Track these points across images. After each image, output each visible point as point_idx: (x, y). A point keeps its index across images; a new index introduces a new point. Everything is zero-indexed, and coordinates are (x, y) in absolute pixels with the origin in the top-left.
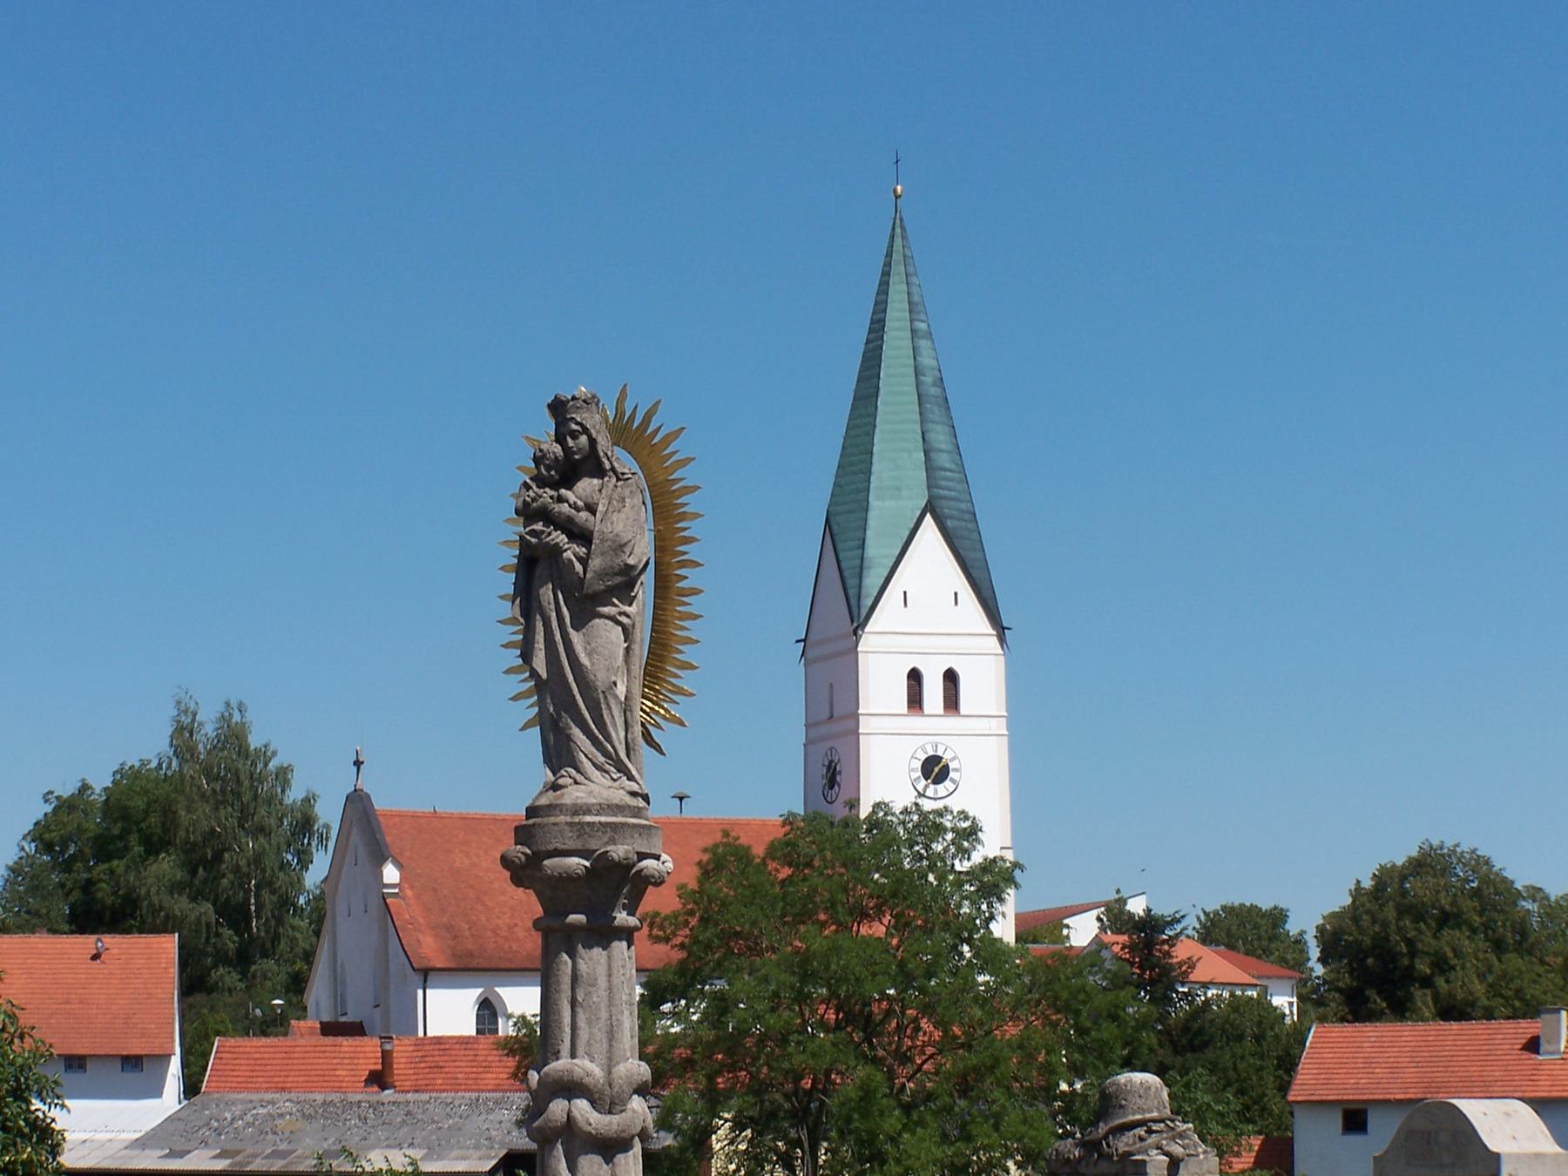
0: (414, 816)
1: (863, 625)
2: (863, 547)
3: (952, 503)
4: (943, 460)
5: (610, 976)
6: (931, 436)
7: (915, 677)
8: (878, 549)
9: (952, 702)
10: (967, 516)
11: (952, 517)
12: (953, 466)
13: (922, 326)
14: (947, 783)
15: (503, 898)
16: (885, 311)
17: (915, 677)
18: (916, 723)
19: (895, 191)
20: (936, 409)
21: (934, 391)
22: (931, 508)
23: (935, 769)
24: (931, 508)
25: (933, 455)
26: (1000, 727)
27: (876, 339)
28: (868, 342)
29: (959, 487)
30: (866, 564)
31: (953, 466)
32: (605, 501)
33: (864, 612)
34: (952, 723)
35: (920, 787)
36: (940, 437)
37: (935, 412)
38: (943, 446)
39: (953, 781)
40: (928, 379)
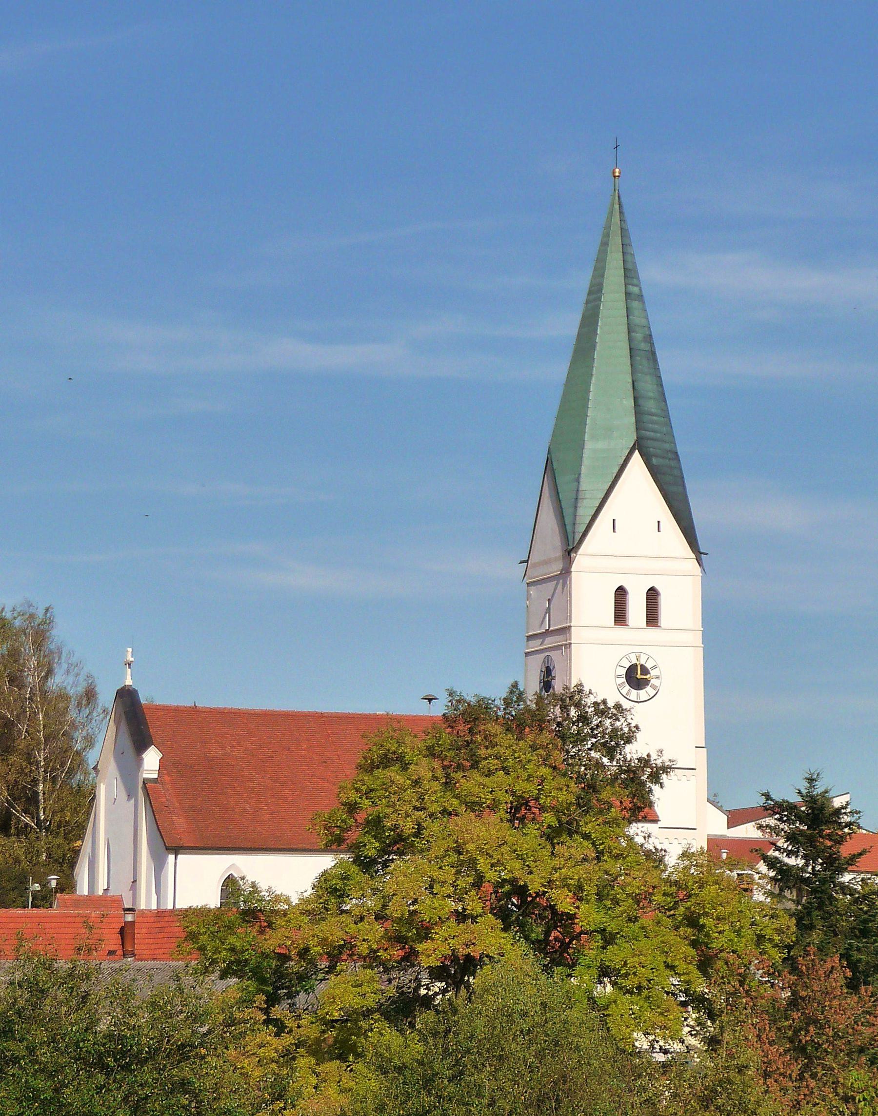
0: (177, 710)
1: (576, 548)
2: (578, 480)
3: (655, 444)
4: (650, 405)
5: (134, 881)
6: (640, 385)
7: (621, 593)
8: (591, 487)
9: (652, 618)
10: (670, 455)
11: (656, 456)
12: (659, 412)
13: (635, 290)
14: (648, 688)
15: (251, 784)
16: (603, 276)
17: (621, 593)
18: (620, 632)
19: (614, 172)
20: (645, 362)
21: (643, 346)
22: (639, 445)
23: (636, 677)
24: (639, 445)
25: (641, 401)
26: (697, 638)
27: (595, 300)
28: (587, 302)
29: (664, 429)
30: (581, 496)
31: (659, 412)
32: (517, 864)
33: (578, 537)
34: (652, 632)
35: (624, 692)
36: (647, 386)
37: (644, 364)
38: (651, 394)
39: (654, 687)
40: (638, 336)
